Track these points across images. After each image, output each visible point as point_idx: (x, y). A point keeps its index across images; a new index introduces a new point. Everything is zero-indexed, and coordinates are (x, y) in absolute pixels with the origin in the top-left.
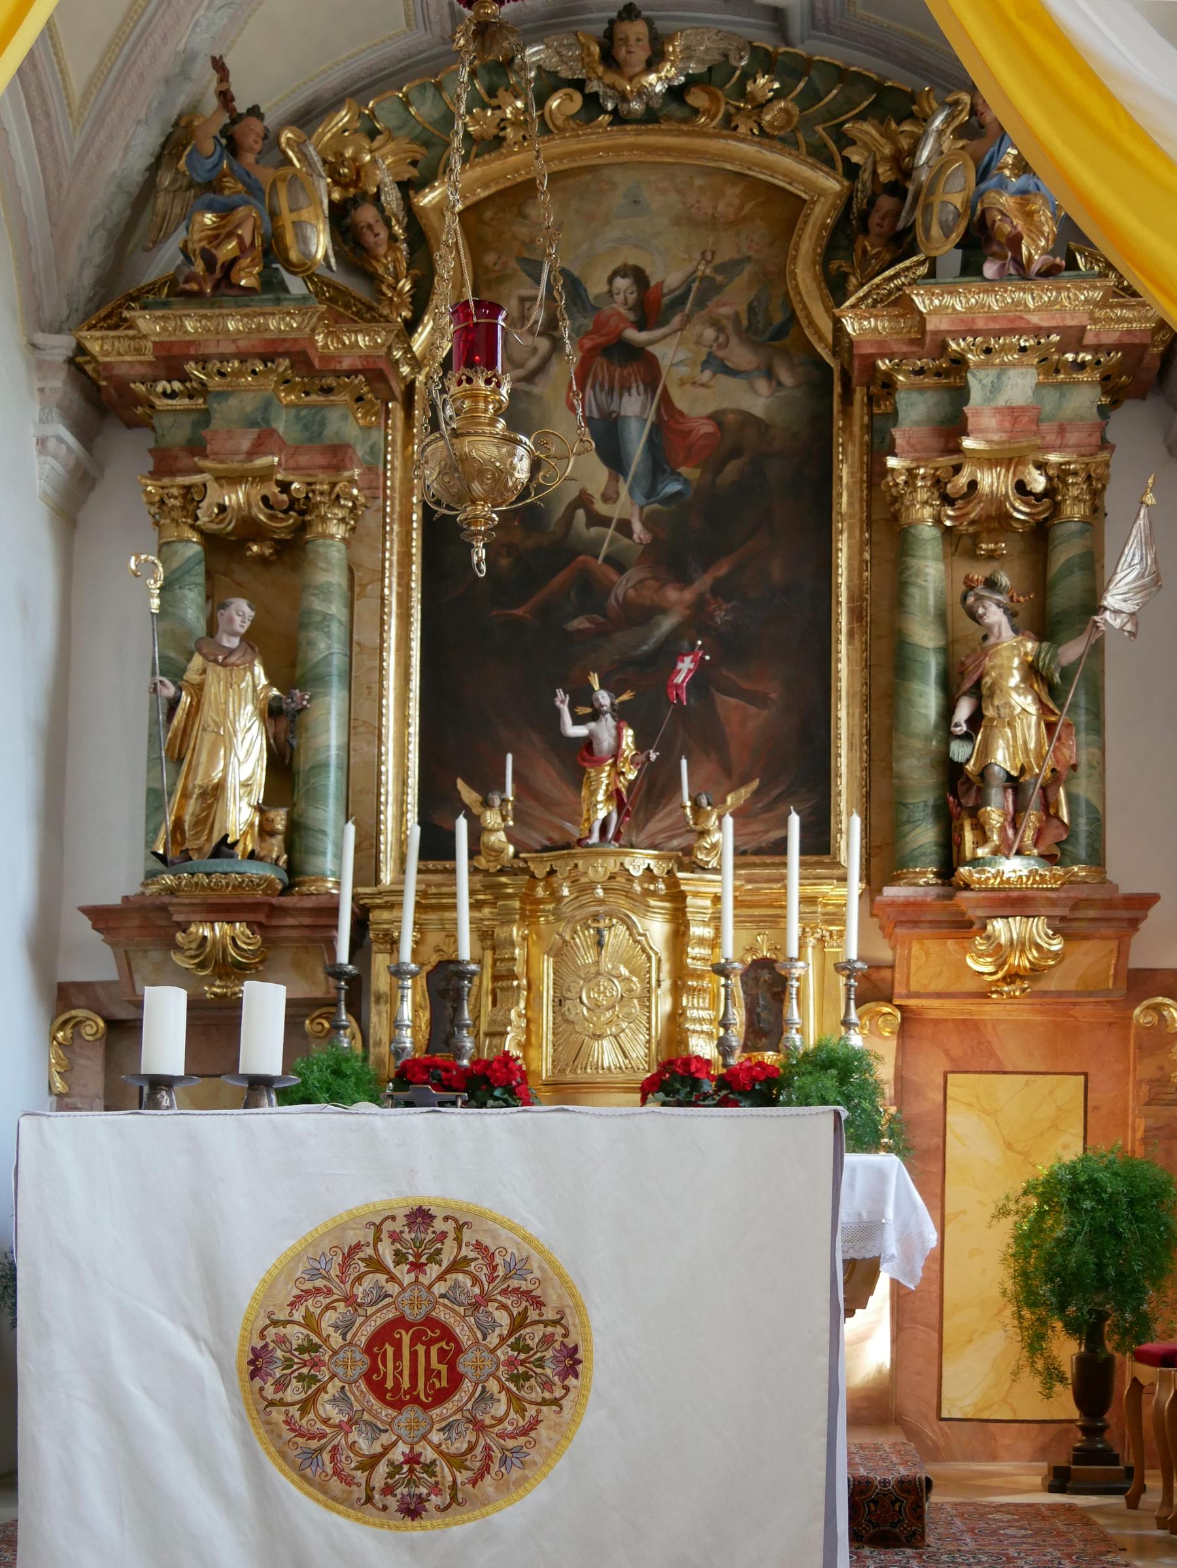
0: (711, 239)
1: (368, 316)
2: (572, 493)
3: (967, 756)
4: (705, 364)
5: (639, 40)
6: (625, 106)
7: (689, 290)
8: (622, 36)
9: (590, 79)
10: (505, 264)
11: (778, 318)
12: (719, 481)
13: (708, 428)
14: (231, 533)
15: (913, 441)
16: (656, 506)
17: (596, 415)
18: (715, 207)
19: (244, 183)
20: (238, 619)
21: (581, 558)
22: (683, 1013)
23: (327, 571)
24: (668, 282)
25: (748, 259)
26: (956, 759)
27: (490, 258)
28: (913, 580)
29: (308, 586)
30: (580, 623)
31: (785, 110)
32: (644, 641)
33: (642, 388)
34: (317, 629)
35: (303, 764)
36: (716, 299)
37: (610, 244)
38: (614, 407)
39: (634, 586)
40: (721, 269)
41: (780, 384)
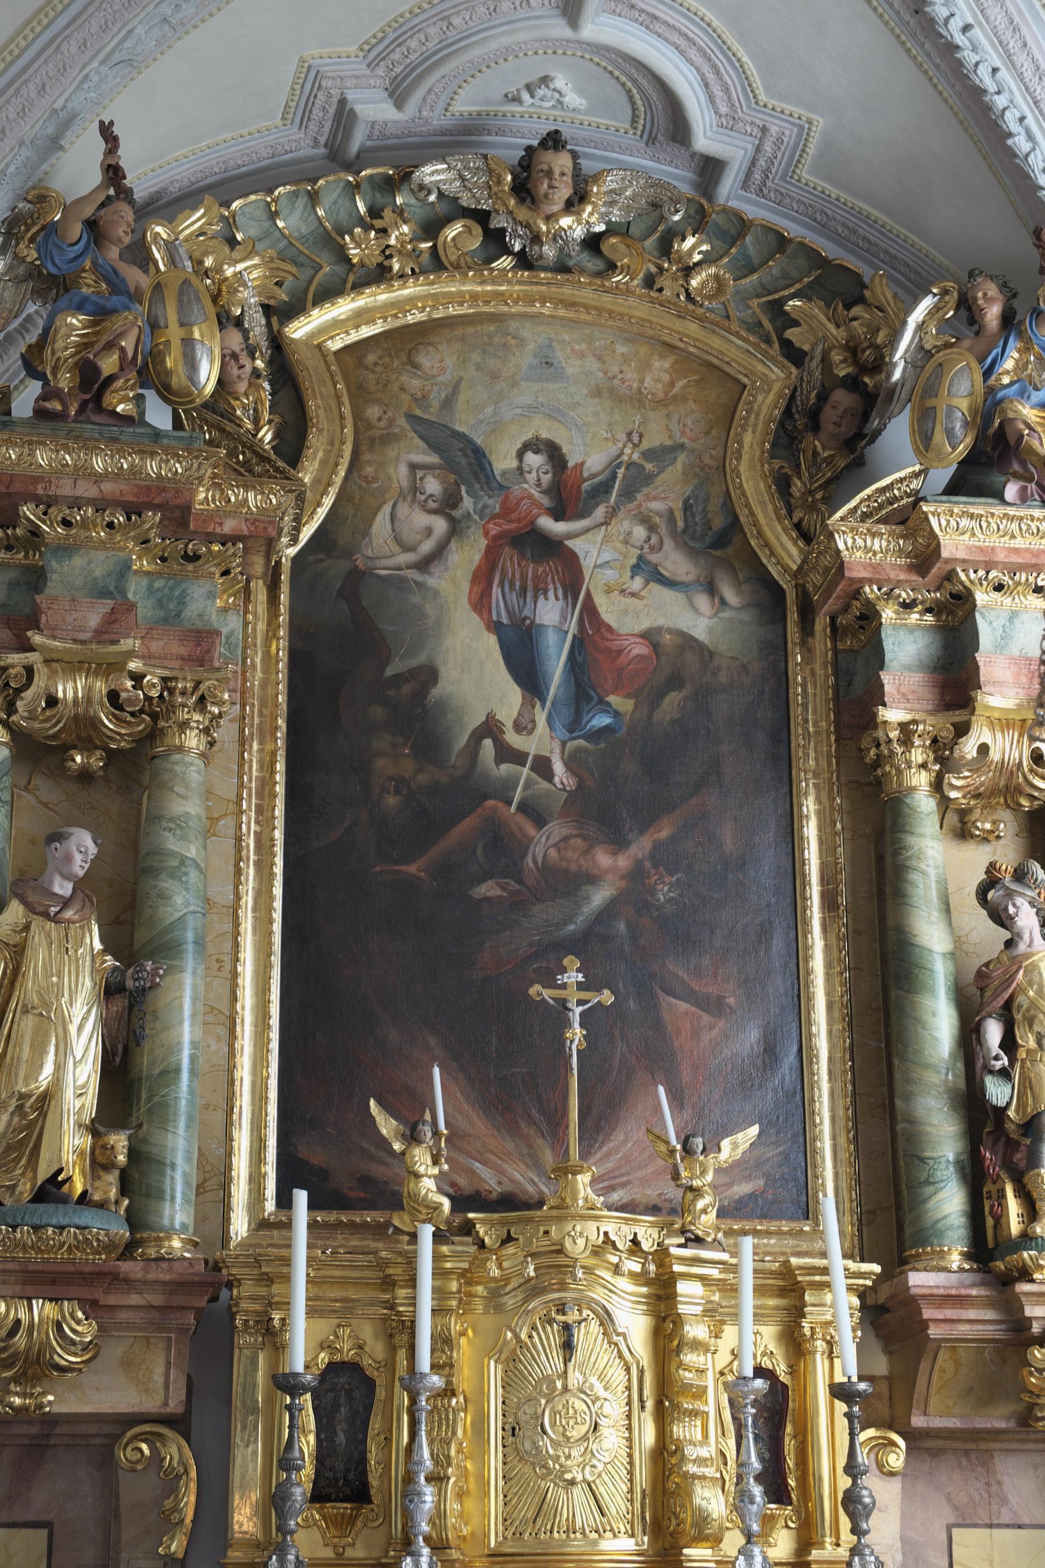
0: (638, 419)
1: (258, 469)
2: (478, 719)
3: (1007, 1099)
4: (636, 569)
5: (563, 174)
6: (536, 248)
7: (614, 476)
8: (545, 167)
9: (497, 212)
10: (392, 422)
11: (718, 522)
12: (657, 716)
13: (640, 649)
14: (54, 737)
15: (903, 689)
16: (581, 742)
17: (505, 620)
18: (642, 381)
19: (109, 282)
20: (78, 858)
21: (490, 803)
22: (679, 1450)
23: (185, 798)
24: (588, 464)
25: (682, 446)
26: (994, 1102)
27: (373, 412)
28: (913, 863)
29: (160, 817)
30: (488, 889)
31: (717, 278)
32: (569, 919)
33: (560, 592)
34: (172, 876)
35: (145, 1061)
36: (646, 490)
37: (519, 411)
38: (526, 612)
39: (556, 845)
40: (649, 455)
41: (723, 602)
